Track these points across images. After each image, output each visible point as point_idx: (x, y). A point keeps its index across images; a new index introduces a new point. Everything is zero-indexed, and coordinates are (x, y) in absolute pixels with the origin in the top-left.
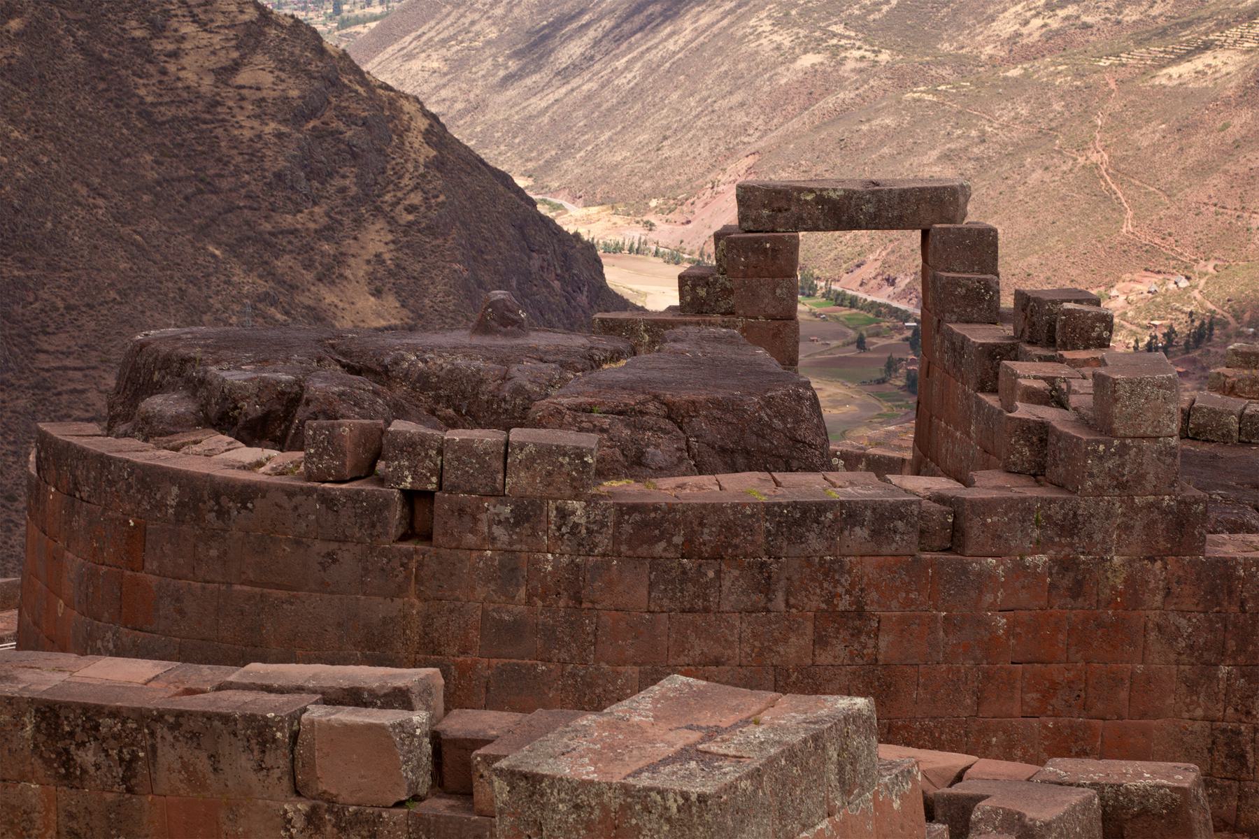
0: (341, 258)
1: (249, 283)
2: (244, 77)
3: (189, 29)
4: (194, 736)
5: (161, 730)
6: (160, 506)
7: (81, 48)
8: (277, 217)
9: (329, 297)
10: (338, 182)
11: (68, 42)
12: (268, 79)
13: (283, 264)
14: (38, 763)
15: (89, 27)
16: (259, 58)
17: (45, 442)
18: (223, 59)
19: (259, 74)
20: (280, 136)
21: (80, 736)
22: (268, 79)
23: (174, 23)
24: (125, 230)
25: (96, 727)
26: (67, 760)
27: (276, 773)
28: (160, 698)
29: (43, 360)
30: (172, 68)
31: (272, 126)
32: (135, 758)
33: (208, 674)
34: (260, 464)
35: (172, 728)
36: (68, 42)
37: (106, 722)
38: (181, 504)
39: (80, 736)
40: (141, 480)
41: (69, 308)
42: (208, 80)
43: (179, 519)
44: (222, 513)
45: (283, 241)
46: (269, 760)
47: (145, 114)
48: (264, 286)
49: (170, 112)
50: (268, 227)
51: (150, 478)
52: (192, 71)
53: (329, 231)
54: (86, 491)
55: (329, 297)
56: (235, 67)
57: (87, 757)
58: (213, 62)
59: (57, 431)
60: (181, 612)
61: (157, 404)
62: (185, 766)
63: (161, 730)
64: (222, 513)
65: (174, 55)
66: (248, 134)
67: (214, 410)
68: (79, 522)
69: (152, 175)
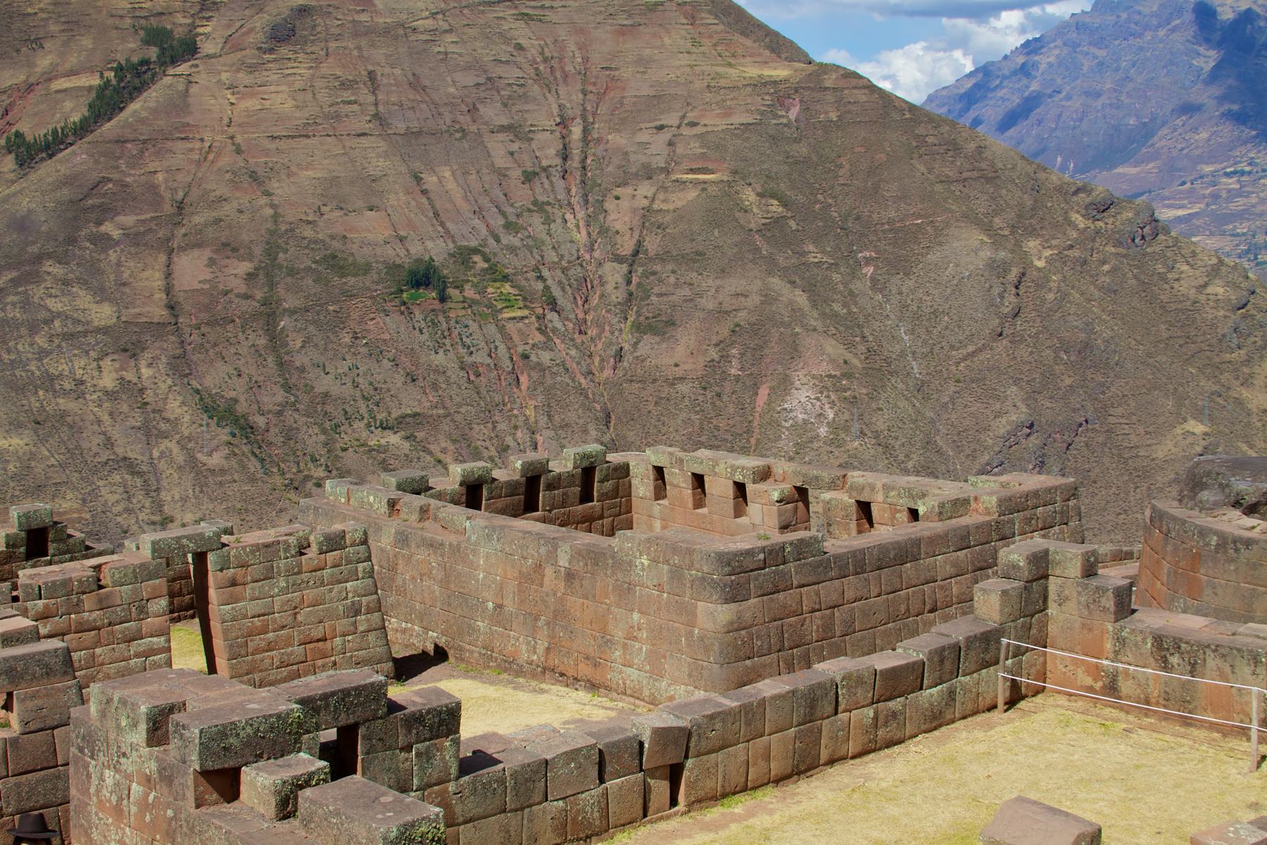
0: (1252, 375)
1: (1209, 386)
2: (1210, 290)
3: (1185, 268)
4: (1223, 656)
5: (1208, 652)
6: (1208, 544)
7: (1135, 277)
8: (1222, 355)
9: (1245, 393)
10: (1252, 339)
11: (1130, 275)
12: (1221, 290)
13: (1224, 378)
14: (1152, 660)
15: (1138, 268)
16: (1217, 281)
17: (1154, 508)
18: (1201, 281)
19: (1217, 289)
20: (1225, 317)
21: (1172, 651)
22: (1221, 290)
23: (1178, 265)
24: (1151, 361)
25: (1179, 647)
26: (1165, 660)
27: (1261, 677)
28: (1205, 636)
29: (1111, 419)
30: (1176, 285)
31: (1222, 313)
32: (1196, 663)
33: (1230, 626)
34: (1253, 527)
35: (1214, 651)
36: (1130, 275)
37: (1183, 646)
38: (1218, 545)
39: (1172, 651)
40: (1200, 532)
41: (1124, 396)
42: (1193, 291)
43: (1217, 551)
44: (1237, 550)
45: (1224, 366)
46: (1258, 671)
47: (1163, 307)
48: (1215, 388)
49: (1173, 306)
50: (1217, 360)
51: (1203, 532)
52: (1185, 288)
53: (1248, 362)
54: (1173, 534)
55: (1245, 393)
56: (1205, 285)
57: (1174, 660)
58: (1196, 283)
59: (1160, 505)
60: (1216, 594)
61: (1205, 495)
62: (1219, 669)
63: (1208, 652)
64: (1237, 550)
65: (1177, 280)
66: (1210, 316)
67: (1233, 499)
68: (1169, 548)
69: (1165, 335)
